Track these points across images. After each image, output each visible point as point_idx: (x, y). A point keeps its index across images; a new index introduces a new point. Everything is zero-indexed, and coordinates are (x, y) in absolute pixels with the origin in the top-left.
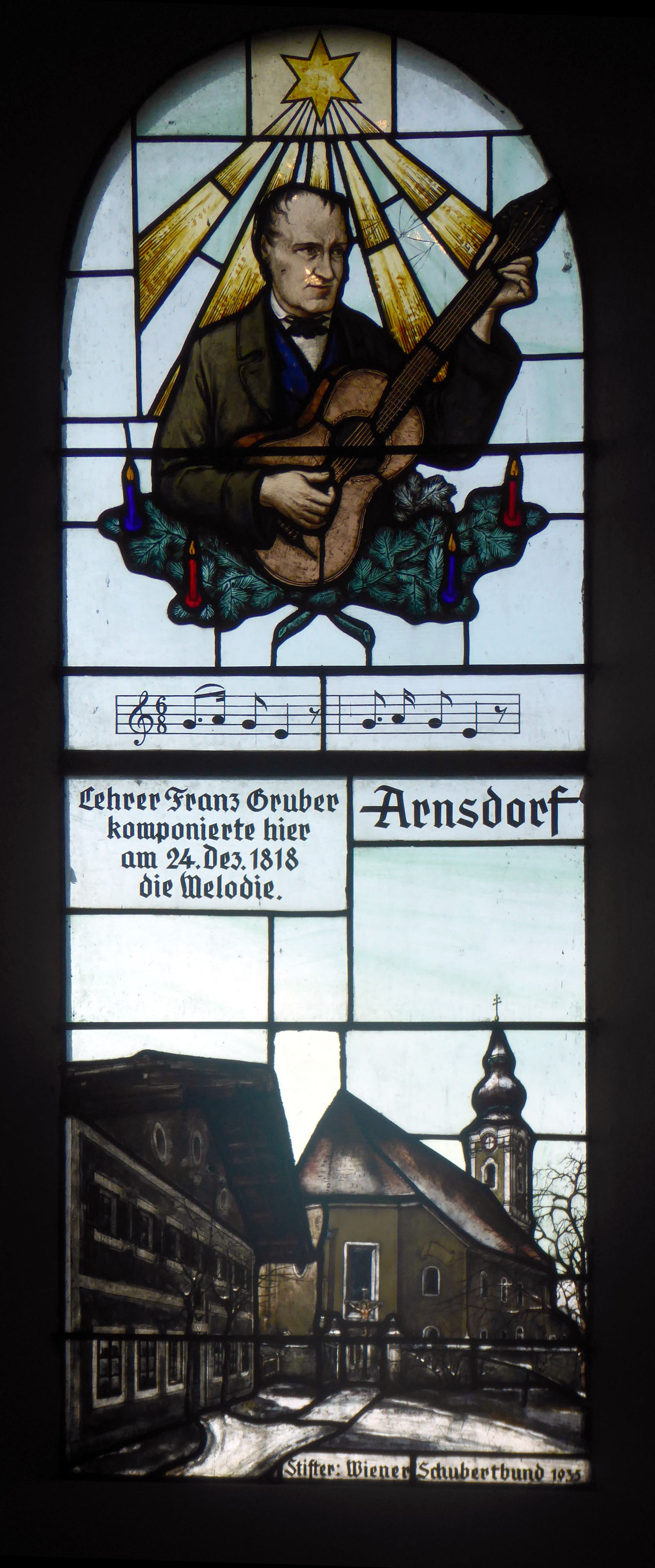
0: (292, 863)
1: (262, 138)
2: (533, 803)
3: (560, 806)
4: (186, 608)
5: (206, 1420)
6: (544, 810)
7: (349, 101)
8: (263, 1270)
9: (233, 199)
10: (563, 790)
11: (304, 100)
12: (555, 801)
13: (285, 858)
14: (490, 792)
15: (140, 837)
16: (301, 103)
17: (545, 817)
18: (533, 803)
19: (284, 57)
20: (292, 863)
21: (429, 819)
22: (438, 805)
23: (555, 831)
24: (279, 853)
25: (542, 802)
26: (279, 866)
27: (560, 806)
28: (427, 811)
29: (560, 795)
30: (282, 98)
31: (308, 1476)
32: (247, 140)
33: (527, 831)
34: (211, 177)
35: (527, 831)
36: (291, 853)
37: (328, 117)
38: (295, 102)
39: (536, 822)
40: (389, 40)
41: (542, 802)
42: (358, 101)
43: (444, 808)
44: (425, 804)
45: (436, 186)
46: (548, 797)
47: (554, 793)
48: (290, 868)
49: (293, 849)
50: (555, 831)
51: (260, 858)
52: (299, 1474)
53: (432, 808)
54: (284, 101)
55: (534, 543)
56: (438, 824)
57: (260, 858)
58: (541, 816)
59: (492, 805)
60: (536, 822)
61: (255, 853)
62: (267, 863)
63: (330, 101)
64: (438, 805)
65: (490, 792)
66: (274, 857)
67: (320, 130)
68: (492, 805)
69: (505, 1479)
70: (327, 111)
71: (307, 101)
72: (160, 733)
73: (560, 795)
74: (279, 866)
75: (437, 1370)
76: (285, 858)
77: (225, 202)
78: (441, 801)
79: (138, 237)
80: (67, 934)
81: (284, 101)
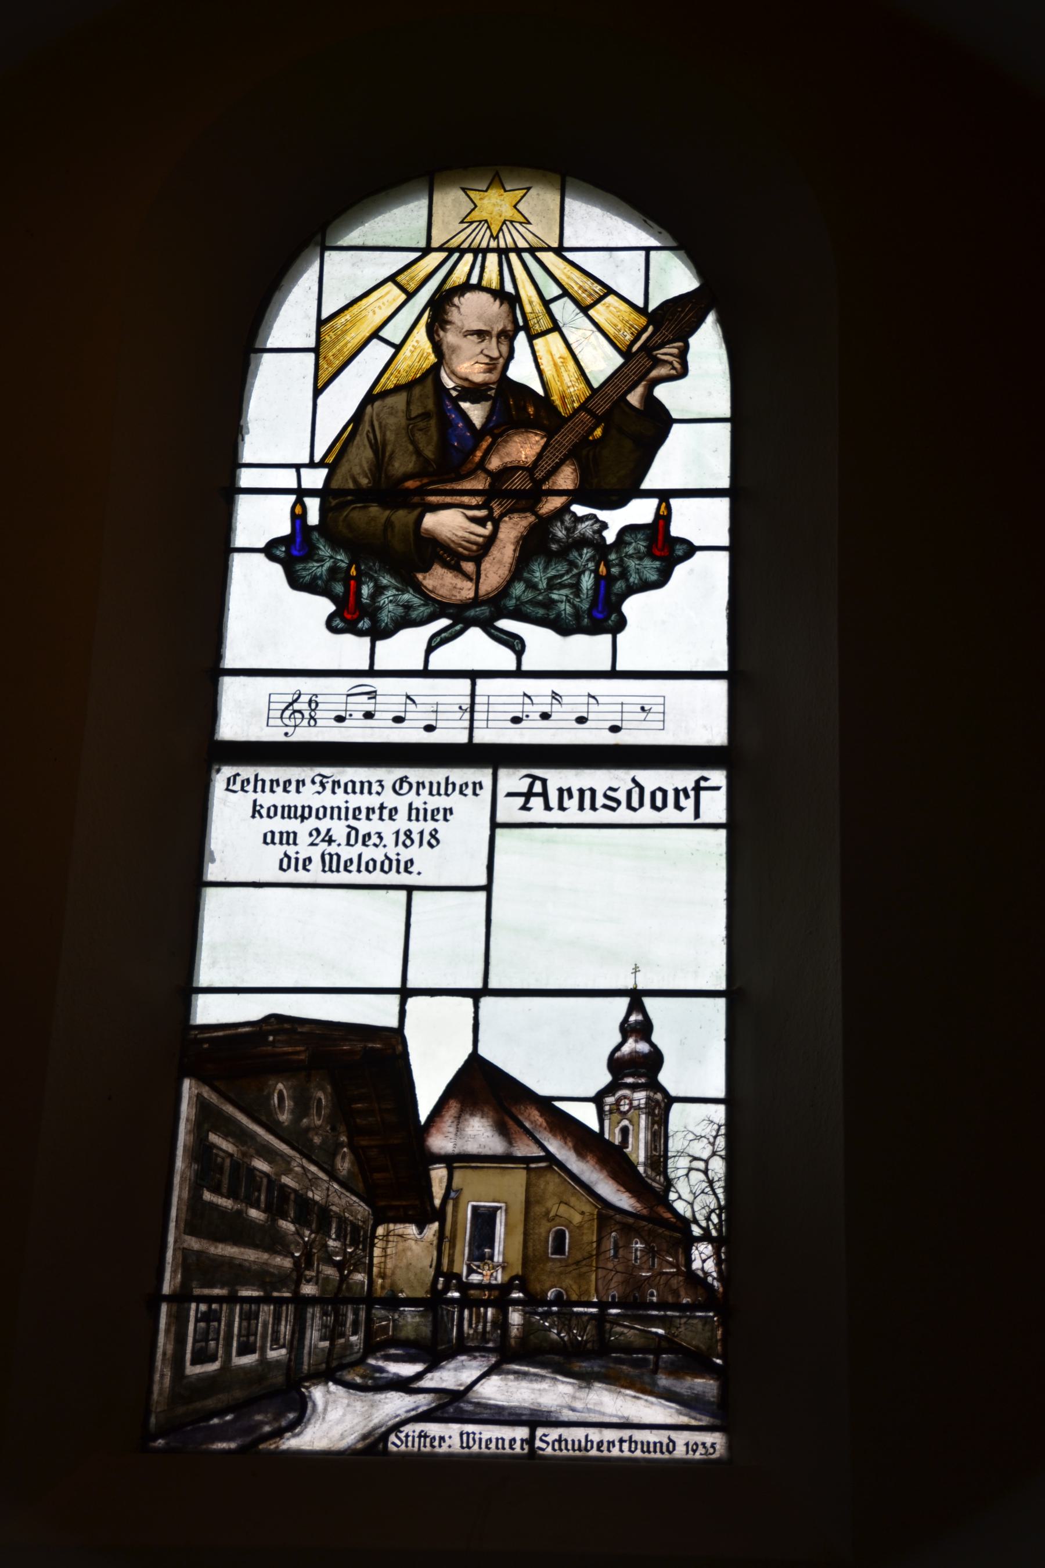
0: (433, 842)
1: (440, 249)
3: (703, 794)
4: (343, 619)
5: (307, 1388)
6: (687, 796)
7: (521, 223)
8: (380, 1231)
9: (410, 295)
11: (480, 222)
12: (698, 789)
13: (427, 837)
16: (477, 223)
17: (688, 804)
19: (464, 190)
20: (433, 842)
21: (572, 804)
22: (581, 792)
23: (697, 815)
24: (422, 833)
25: (685, 790)
27: (703, 794)
29: (703, 784)
32: (427, 251)
33: (687, 816)
35: (670, 815)
37: (501, 235)
38: (471, 223)
39: (678, 807)
40: (557, 178)
42: (529, 223)
43: (588, 795)
46: (690, 785)
47: (697, 782)
49: (436, 831)
50: (697, 815)
51: (402, 837)
53: (576, 794)
54: (462, 222)
55: (680, 571)
56: (581, 808)
57: (402, 837)
58: (683, 802)
60: (678, 807)
62: (408, 842)
65: (634, 780)
66: (416, 837)
67: (493, 244)
70: (501, 229)
72: (310, 726)
73: (703, 784)
77: (611, 299)
78: (585, 788)
79: (321, 323)
81: (462, 222)
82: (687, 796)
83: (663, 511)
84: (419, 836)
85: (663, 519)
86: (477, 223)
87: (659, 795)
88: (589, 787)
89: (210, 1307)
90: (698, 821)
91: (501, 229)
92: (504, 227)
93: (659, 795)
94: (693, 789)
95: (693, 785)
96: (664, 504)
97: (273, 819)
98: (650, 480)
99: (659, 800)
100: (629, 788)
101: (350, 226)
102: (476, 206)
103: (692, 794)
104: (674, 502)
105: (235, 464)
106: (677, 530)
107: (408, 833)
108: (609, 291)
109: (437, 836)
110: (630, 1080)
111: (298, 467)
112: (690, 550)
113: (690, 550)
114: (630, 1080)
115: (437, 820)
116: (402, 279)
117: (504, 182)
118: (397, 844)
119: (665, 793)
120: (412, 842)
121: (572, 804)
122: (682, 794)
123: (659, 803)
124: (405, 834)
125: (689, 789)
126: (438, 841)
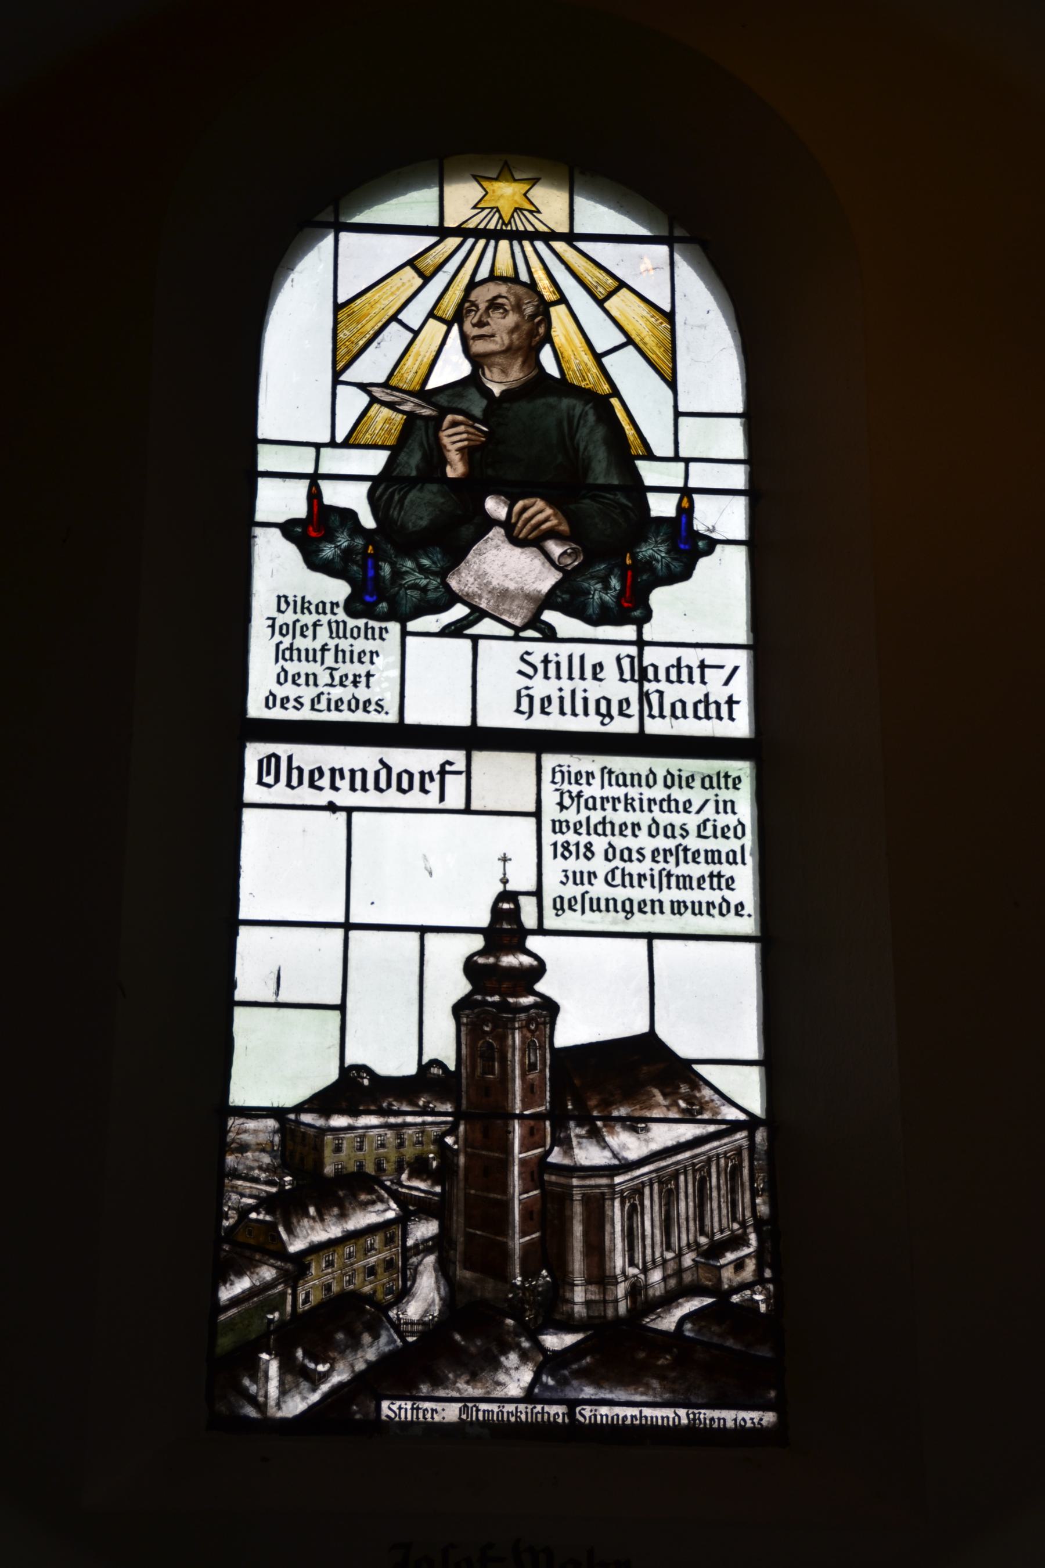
0: (589, 854)
2: (422, 774)
3: (448, 777)
6: (432, 779)
7: (531, 212)
9: (427, 279)
10: (451, 764)
11: (492, 208)
12: (443, 772)
13: (582, 850)
14: (381, 761)
15: (719, 852)
16: (489, 210)
17: (433, 787)
18: (422, 774)
20: (589, 854)
21: (344, 784)
23: (442, 798)
26: (578, 857)
28: (342, 777)
29: (448, 768)
30: (472, 206)
31: (409, 1418)
33: (431, 801)
34: (411, 263)
36: (588, 846)
37: (512, 220)
38: (483, 209)
39: (424, 790)
41: (430, 773)
42: (538, 212)
43: (359, 776)
44: (341, 771)
45: (610, 281)
46: (436, 769)
47: (443, 766)
48: (588, 859)
49: (590, 843)
50: (442, 798)
51: (560, 850)
52: (400, 1418)
53: (347, 775)
55: (703, 563)
56: (353, 789)
57: (560, 850)
58: (428, 785)
59: (383, 774)
60: (424, 790)
61: (555, 844)
62: (566, 854)
63: (516, 210)
64: (353, 772)
65: (381, 761)
66: (573, 848)
68: (383, 774)
69: (475, 1406)
70: (512, 216)
71: (495, 210)
73: (448, 768)
74: (578, 857)
75: (675, 1350)
76: (582, 850)
78: (356, 769)
79: (337, 307)
80: (760, 956)
81: (475, 207)
82: (432, 779)
83: (685, 504)
84: (575, 847)
85: (686, 512)
86: (489, 210)
87: (405, 778)
88: (360, 767)
89: (411, 1393)
90: (441, 806)
91: (512, 216)
92: (515, 215)
93: (405, 778)
94: (439, 773)
95: (438, 769)
96: (685, 500)
97: (730, 849)
98: (263, 418)
99: (405, 781)
100: (376, 769)
101: (361, 207)
102: (487, 193)
103: (437, 777)
104: (696, 497)
105: (250, 442)
106: (700, 525)
107: (565, 845)
108: (622, 284)
109: (592, 849)
110: (623, 1111)
111: (318, 446)
112: (711, 545)
113: (711, 545)
114: (623, 1111)
115: (580, 834)
116: (601, 292)
117: (513, 170)
118: (555, 856)
119: (411, 776)
120: (571, 853)
121: (344, 784)
122: (427, 777)
123: (405, 785)
124: (563, 845)
125: (435, 772)
126: (593, 854)
